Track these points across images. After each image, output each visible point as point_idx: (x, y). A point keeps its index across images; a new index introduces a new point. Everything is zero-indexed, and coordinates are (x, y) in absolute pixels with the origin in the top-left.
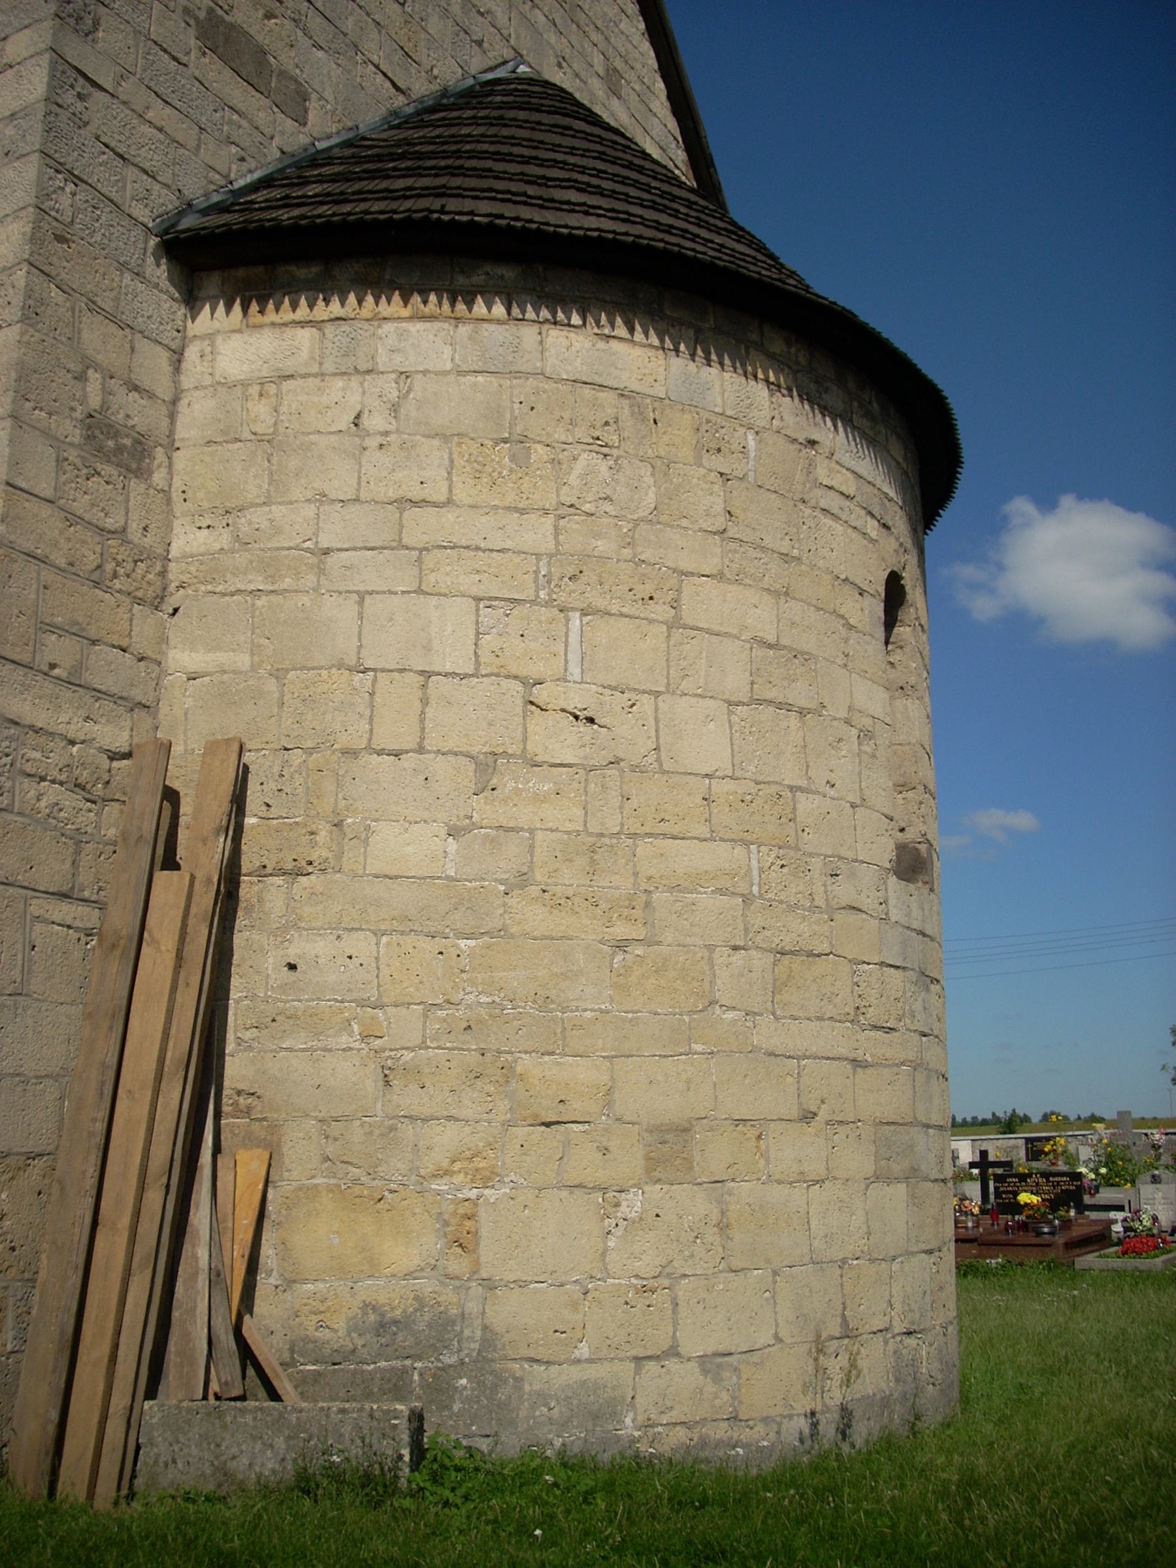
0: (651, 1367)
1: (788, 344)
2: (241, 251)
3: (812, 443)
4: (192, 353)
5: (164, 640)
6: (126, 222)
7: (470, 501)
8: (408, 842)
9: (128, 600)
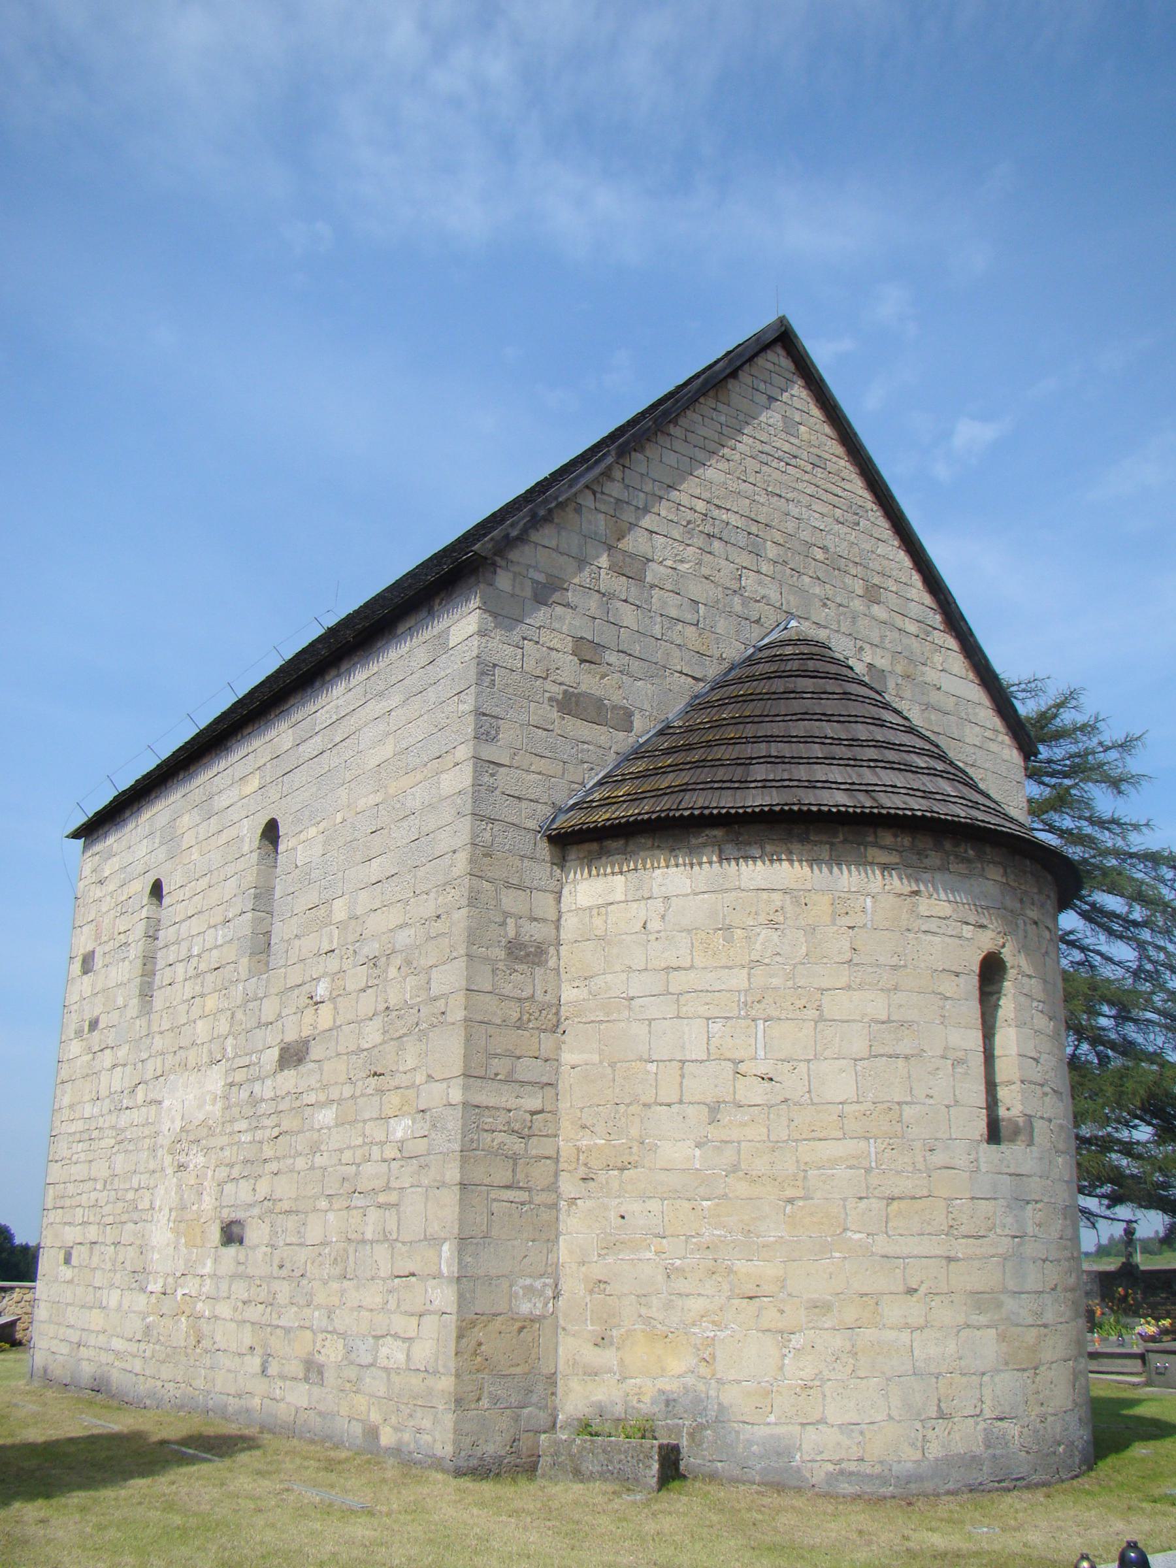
1: (896, 836)
2: (583, 839)
4: (565, 892)
6: (523, 832)
7: (702, 965)
9: (537, 1032)
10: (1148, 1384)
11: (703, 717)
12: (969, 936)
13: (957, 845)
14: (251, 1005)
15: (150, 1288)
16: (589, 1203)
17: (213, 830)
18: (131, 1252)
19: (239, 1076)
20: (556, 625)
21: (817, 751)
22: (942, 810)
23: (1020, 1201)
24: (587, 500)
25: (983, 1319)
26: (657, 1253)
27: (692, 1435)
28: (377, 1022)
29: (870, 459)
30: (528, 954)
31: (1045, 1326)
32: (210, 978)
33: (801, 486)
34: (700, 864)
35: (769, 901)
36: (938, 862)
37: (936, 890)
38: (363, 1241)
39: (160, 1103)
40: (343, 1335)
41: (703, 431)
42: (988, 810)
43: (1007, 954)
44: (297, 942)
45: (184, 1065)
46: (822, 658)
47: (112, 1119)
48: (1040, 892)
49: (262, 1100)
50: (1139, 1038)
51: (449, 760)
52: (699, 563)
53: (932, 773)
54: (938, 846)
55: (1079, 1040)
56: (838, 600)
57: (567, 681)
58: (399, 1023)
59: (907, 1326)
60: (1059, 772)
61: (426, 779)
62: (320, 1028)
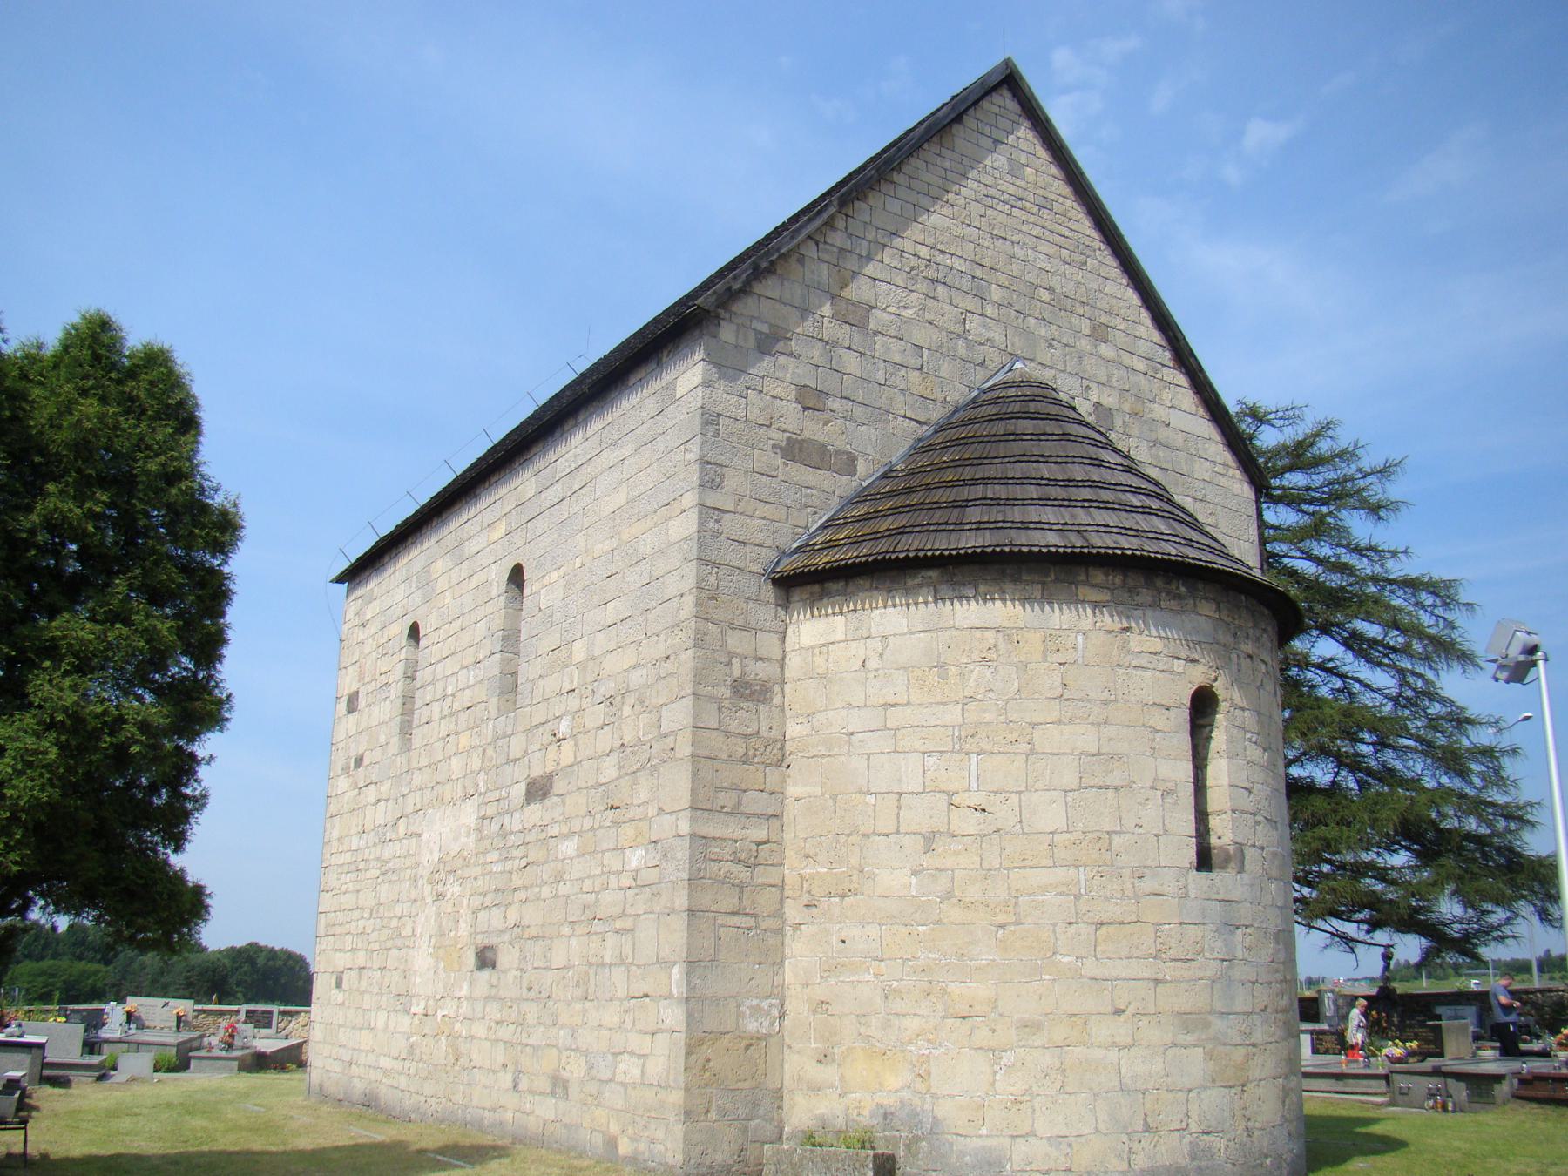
1: (1107, 575)
2: (806, 581)
6: (748, 576)
10: (1392, 1103)
11: (924, 461)
12: (1180, 670)
13: (1168, 583)
14: (500, 742)
16: (813, 929)
17: (464, 574)
18: (396, 976)
19: (491, 810)
20: (779, 374)
21: (1033, 492)
22: (1152, 548)
23: (1230, 926)
24: (810, 251)
25: (1189, 1039)
26: (875, 975)
27: (908, 1146)
28: (612, 760)
29: (1097, 199)
30: (752, 693)
31: (1254, 1045)
32: (463, 716)
33: (1026, 228)
34: (916, 604)
35: (982, 639)
36: (1149, 599)
37: (1147, 626)
38: (603, 965)
39: (419, 835)
40: (586, 1053)
41: (926, 177)
42: (1202, 547)
43: (1220, 688)
44: (541, 682)
45: (441, 799)
46: (1044, 399)
47: (376, 851)
48: (1255, 626)
50: (1398, 765)
51: (677, 506)
52: (923, 309)
53: (1147, 511)
54: (1149, 584)
55: (1338, 767)
56: (1065, 340)
57: (790, 427)
58: (633, 759)
59: (1114, 1045)
60: (1317, 500)
61: (656, 525)
62: (563, 763)
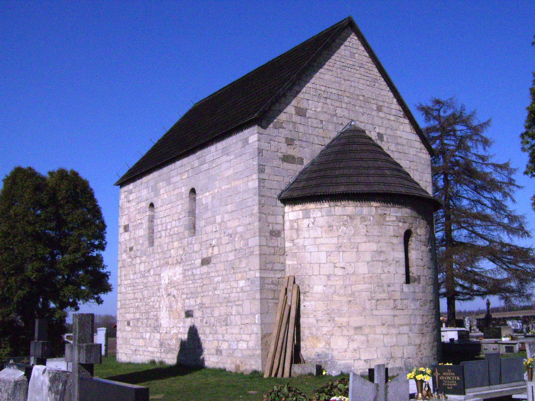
0: (356, 361)
3: (385, 214)
5: (285, 259)
8: (318, 288)
15: (161, 332)
20: (280, 135)
30: (276, 234)
46: (361, 137)
49: (196, 275)
52: (323, 108)
56: (368, 113)
